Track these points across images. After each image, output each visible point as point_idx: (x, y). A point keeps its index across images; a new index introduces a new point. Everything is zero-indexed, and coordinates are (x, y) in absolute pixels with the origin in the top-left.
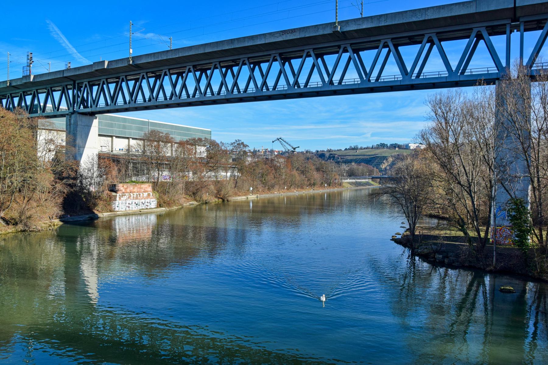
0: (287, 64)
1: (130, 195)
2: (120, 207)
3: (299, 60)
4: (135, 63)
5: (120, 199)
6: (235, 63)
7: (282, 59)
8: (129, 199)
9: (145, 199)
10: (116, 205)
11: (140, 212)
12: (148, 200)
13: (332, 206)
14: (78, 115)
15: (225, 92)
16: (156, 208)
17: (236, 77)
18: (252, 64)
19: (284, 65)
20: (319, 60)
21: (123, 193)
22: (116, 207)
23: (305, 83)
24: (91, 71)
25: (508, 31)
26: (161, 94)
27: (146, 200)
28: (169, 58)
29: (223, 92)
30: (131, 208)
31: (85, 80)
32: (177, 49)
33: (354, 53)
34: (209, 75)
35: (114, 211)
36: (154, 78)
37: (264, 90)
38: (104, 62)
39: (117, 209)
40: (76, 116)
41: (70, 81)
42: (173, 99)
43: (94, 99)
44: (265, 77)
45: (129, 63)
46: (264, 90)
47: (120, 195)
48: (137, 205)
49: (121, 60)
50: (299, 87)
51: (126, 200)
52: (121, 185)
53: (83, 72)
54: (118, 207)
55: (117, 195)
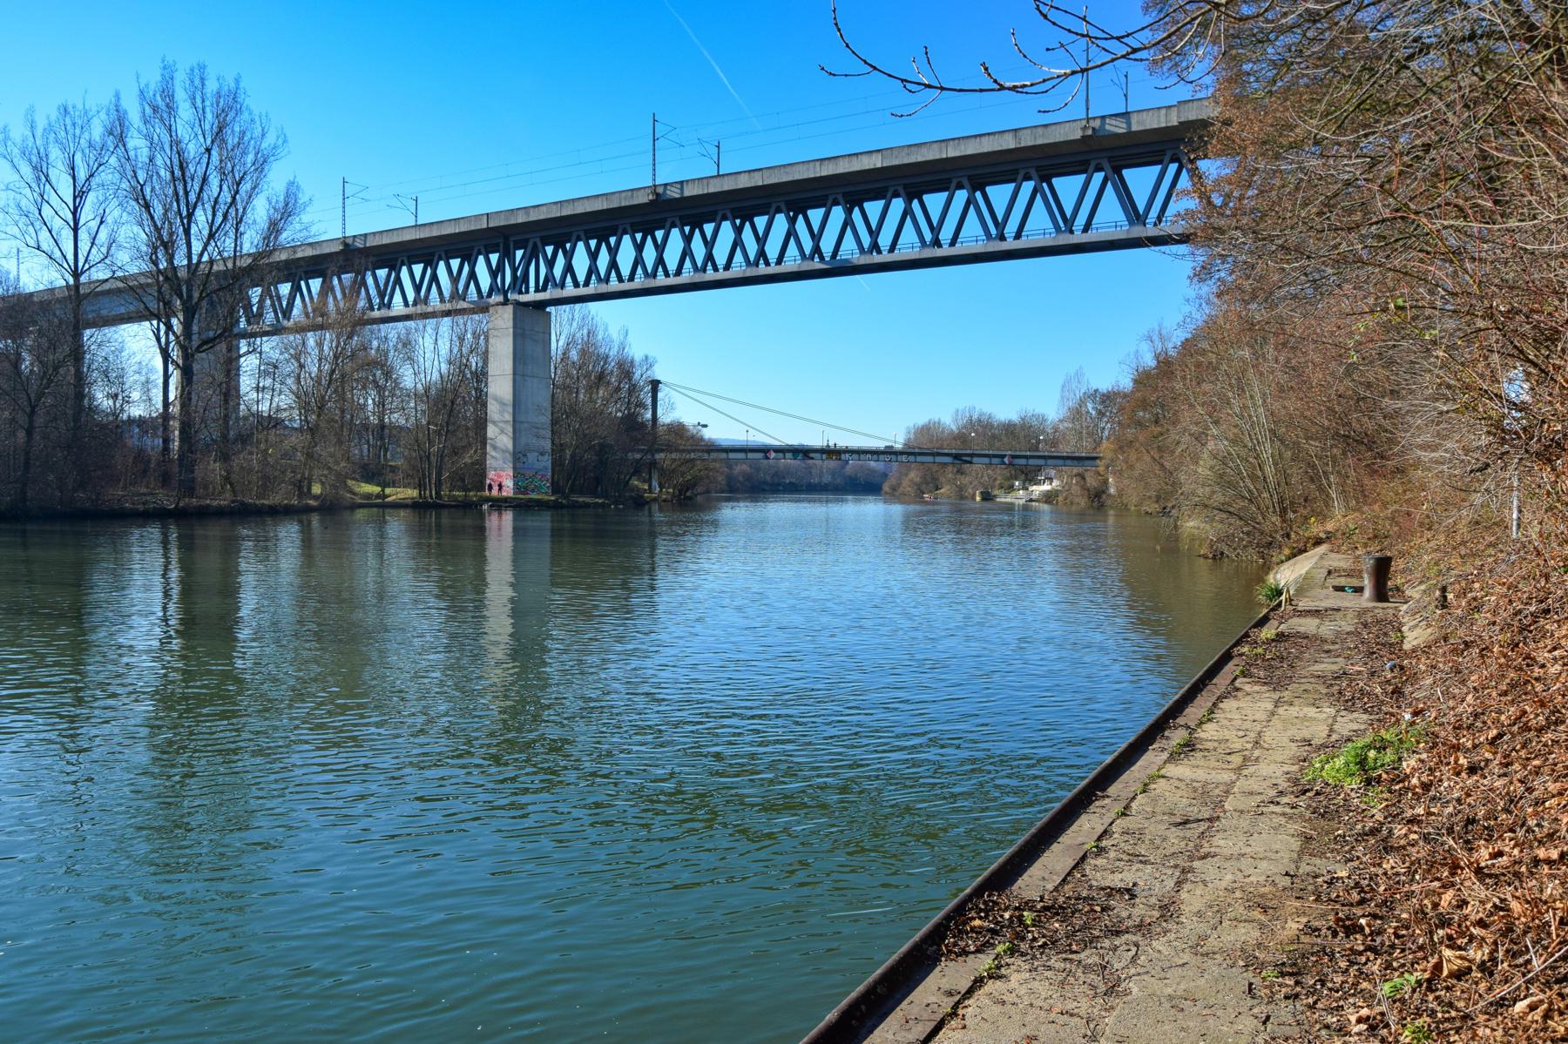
0: (856, 210)
3: (881, 204)
13: (903, 541)
17: (660, 248)
18: (592, 238)
20: (856, 212)
25: (1166, 161)
33: (1042, 181)
43: (472, 283)
44: (761, 241)
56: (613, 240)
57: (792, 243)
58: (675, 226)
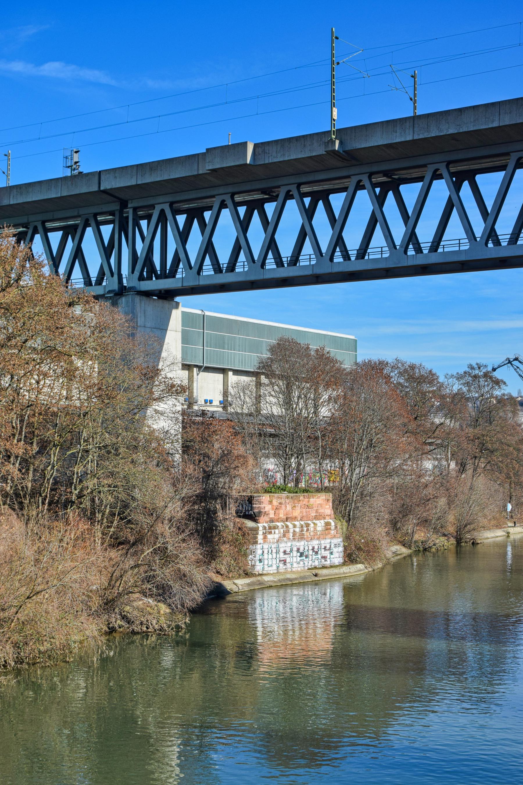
0: (466, 186)
1: (287, 526)
2: (266, 562)
4: (349, 148)
5: (265, 538)
6: (390, 177)
7: (452, 175)
8: (285, 539)
9: (318, 539)
10: (258, 558)
11: (316, 575)
12: (325, 543)
14: (137, 299)
15: (313, 256)
16: (344, 564)
19: (458, 187)
20: (466, 188)
21: (272, 521)
22: (258, 563)
23: (433, 242)
24: (195, 173)
26: (77, 273)
27: (322, 542)
28: (464, 129)
29: (242, 264)
30: (288, 565)
31: (161, 199)
32: (493, 104)
34: (270, 217)
35: (254, 575)
36: (62, 232)
37: (338, 258)
38: (244, 145)
39: (259, 568)
40: (133, 301)
41: (114, 202)
42: (104, 284)
45: (330, 148)
46: (338, 258)
47: (264, 528)
48: (301, 555)
49: (297, 139)
50: (497, 243)
51: (278, 541)
52: (265, 498)
53: (166, 177)
54: (260, 561)
55: (258, 528)
56: (270, 208)
57: (455, 216)
58: (292, 197)
